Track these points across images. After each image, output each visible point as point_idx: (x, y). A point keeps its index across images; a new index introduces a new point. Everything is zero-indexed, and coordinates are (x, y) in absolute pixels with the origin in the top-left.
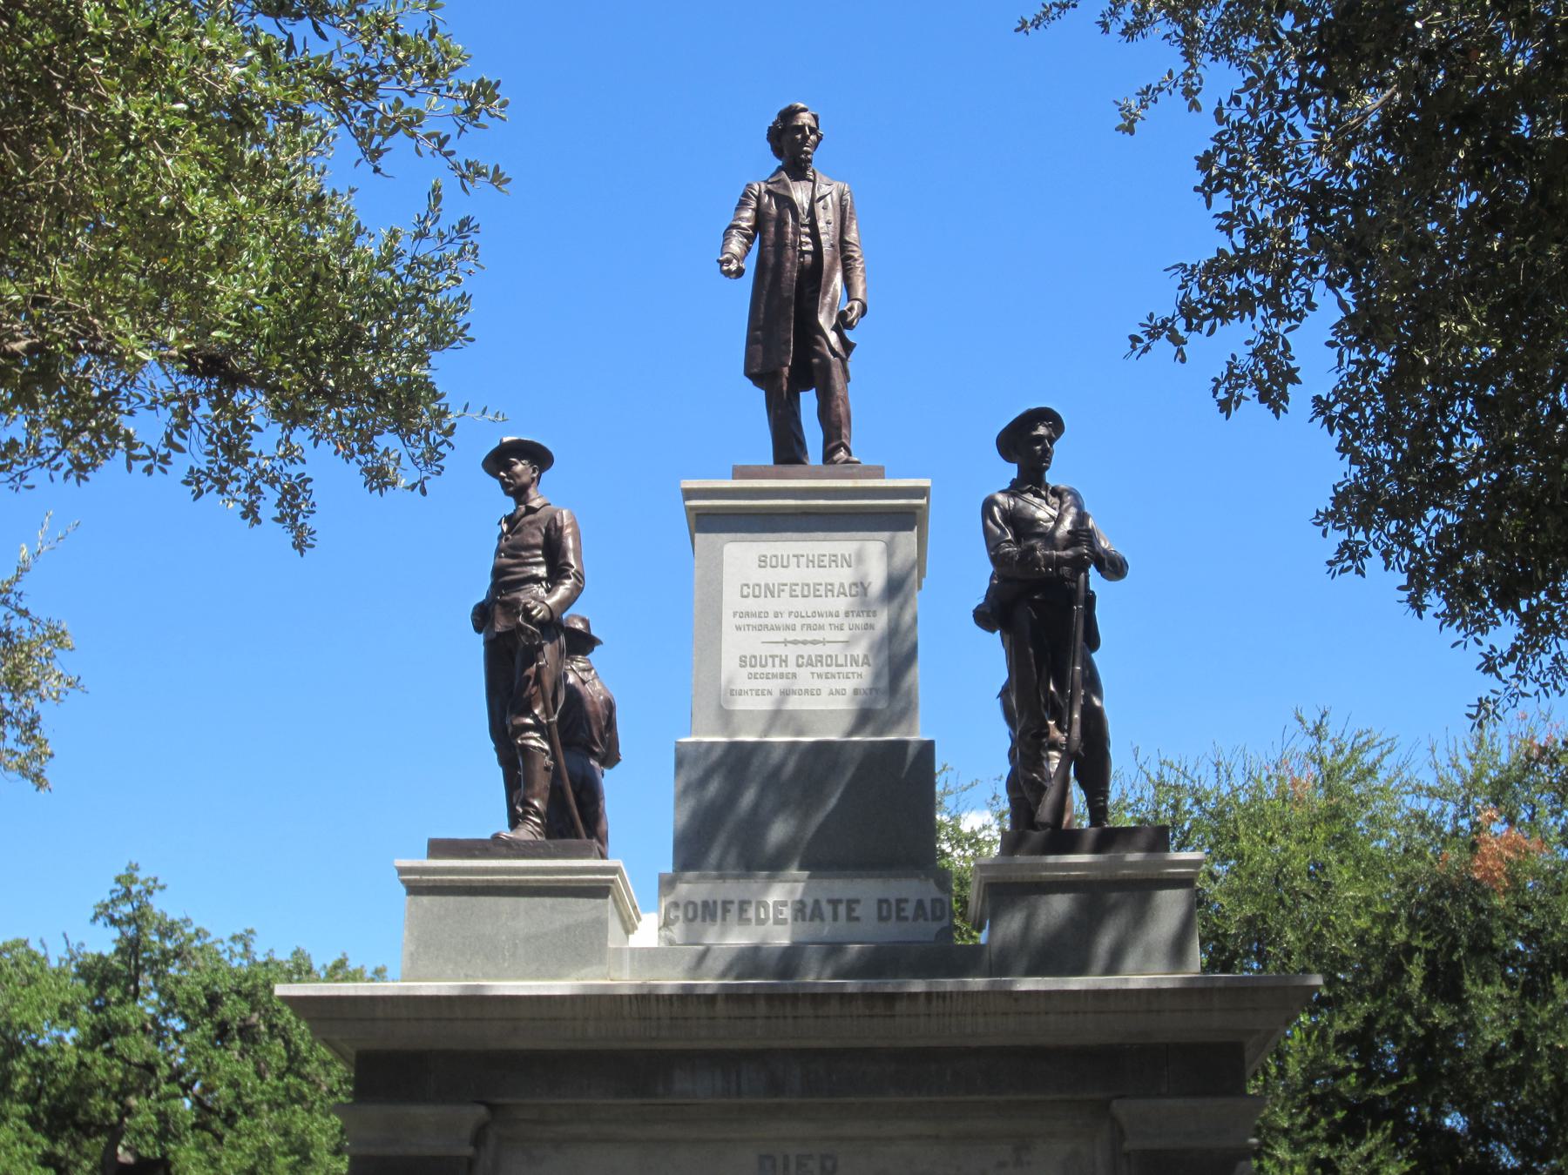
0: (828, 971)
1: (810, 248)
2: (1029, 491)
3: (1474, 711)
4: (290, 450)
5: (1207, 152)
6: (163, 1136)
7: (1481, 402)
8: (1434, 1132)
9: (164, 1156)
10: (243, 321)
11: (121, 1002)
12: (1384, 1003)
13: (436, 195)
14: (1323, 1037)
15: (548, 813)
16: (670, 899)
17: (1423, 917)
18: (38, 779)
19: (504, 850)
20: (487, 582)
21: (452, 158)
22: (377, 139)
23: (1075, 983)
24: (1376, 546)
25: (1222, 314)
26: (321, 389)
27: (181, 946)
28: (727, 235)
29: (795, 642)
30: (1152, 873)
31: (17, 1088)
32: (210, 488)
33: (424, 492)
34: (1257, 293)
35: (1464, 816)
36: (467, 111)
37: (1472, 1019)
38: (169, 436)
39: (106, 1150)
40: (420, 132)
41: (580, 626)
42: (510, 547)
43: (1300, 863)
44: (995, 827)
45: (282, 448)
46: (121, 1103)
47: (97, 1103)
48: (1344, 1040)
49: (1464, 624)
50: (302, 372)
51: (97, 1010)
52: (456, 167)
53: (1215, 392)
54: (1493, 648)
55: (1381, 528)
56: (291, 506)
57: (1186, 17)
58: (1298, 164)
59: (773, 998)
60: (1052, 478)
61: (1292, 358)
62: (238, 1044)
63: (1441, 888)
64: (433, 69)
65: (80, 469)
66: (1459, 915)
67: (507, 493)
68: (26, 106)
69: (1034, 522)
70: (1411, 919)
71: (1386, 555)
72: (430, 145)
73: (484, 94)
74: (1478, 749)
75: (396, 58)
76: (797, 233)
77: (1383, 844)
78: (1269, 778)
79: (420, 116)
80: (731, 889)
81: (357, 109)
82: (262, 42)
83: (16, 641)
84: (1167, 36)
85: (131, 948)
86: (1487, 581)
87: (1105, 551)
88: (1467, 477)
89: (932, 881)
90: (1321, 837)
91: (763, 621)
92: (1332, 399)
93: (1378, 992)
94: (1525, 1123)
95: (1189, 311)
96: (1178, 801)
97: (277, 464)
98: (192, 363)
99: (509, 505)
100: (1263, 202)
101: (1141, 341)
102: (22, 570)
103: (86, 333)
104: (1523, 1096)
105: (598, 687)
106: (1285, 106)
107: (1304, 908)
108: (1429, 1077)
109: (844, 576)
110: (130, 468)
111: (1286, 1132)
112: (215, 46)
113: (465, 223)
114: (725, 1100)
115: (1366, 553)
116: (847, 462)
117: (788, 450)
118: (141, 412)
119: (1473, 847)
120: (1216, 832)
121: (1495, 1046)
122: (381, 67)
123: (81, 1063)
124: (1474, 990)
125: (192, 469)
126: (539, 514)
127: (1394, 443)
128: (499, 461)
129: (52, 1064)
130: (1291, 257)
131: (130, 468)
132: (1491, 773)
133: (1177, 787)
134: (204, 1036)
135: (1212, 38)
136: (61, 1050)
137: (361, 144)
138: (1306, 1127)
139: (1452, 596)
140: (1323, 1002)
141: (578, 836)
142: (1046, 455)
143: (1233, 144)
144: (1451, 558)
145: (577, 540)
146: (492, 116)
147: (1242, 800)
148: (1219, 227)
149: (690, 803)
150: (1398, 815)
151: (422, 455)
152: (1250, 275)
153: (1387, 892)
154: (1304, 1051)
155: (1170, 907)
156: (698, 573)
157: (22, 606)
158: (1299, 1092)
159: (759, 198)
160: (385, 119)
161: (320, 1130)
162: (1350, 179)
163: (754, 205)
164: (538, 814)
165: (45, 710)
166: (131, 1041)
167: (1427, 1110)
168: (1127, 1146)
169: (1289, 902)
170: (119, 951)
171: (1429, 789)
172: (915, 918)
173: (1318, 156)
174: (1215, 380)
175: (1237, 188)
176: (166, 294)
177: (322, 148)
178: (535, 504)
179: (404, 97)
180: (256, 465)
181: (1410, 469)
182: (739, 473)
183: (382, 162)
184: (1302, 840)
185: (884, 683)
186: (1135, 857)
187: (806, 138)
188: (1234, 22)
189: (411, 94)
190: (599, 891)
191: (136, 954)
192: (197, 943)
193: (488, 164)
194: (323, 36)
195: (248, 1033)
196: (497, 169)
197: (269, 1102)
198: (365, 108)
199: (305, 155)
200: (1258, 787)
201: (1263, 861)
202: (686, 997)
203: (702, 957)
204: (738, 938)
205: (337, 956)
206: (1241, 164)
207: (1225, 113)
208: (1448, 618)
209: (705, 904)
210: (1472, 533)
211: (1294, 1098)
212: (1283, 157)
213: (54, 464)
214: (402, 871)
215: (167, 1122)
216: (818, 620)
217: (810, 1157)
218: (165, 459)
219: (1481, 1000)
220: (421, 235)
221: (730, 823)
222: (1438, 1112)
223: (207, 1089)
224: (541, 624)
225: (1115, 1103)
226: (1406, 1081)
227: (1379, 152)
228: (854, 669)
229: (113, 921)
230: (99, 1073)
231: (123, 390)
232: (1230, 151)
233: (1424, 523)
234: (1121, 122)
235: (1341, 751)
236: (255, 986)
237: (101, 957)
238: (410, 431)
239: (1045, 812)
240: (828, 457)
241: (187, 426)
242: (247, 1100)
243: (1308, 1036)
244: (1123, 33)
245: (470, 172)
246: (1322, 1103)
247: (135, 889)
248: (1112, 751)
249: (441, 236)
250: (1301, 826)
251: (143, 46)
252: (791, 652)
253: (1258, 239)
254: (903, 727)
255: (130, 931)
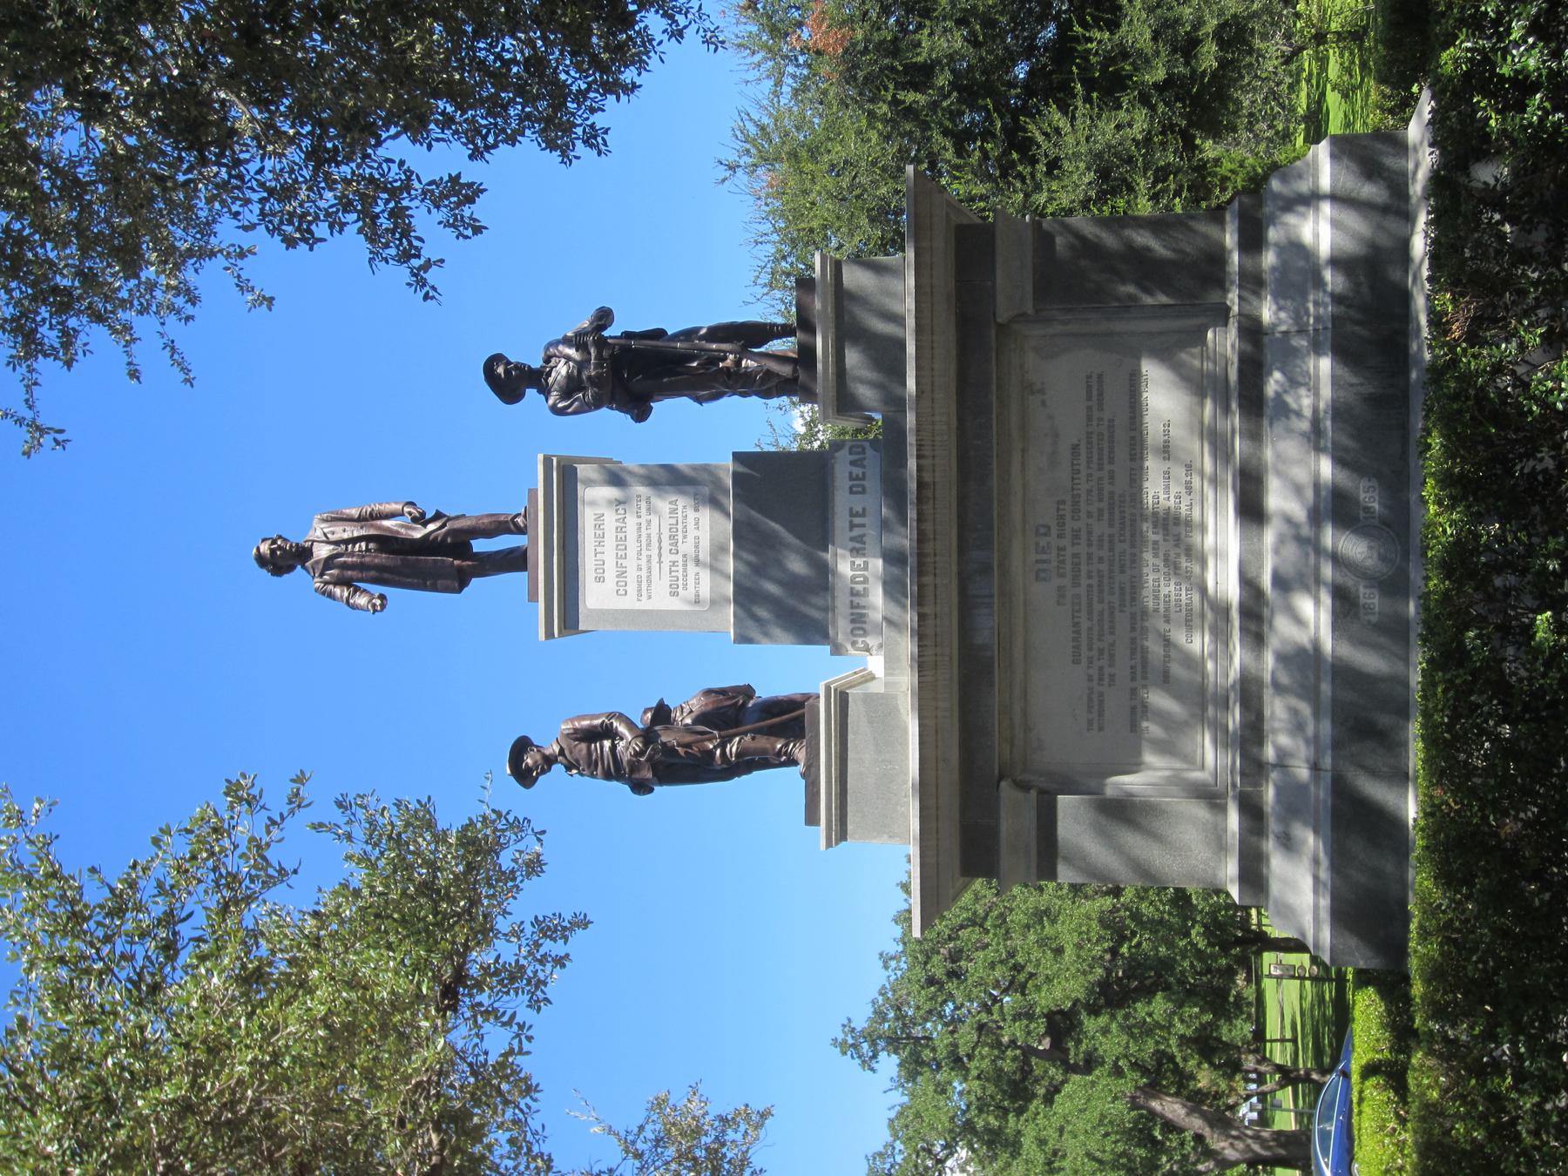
0: (902, 530)
1: (363, 545)
2: (546, 380)
3: (712, 47)
4: (514, 933)
5: (282, 241)
6: (1030, 1016)
7: (480, 33)
8: (1029, 88)
9: (1046, 1016)
10: (414, 970)
11: (934, 1050)
12: (933, 121)
13: (318, 827)
14: (958, 168)
15: (786, 737)
16: (849, 647)
17: (870, 91)
18: (764, 1115)
19: (813, 769)
20: (615, 784)
21: (285, 814)
22: (271, 871)
23: (911, 349)
24: (587, 119)
25: (406, 232)
26: (467, 911)
27: (892, 1007)
28: (354, 607)
29: (660, 555)
30: (830, 291)
31: (997, 1124)
32: (543, 992)
33: (543, 832)
34: (392, 205)
35: (797, 60)
36: (249, 804)
37: (946, 57)
38: (504, 1024)
39: (1041, 1058)
40: (266, 839)
41: (649, 715)
42: (589, 767)
43: (829, 182)
44: (802, 408)
45: (512, 939)
46: (1007, 1048)
47: (1008, 1066)
48: (960, 152)
49: (647, 53)
50: (453, 925)
51: (939, 1067)
52: (292, 812)
53: (467, 237)
54: (665, 31)
55: (573, 114)
56: (556, 931)
57: (181, 255)
58: (292, 171)
59: (920, 571)
60: (536, 363)
61: (441, 179)
62: (962, 963)
63: (850, 79)
64: (215, 830)
65: (529, 1089)
66: (869, 64)
67: (549, 769)
68: (249, 1139)
69: (569, 376)
70: (872, 101)
71: (593, 111)
72: (275, 832)
73: (236, 791)
74: (746, 48)
75: (207, 859)
76: (352, 554)
77: (816, 120)
78: (767, 205)
79: (252, 839)
80: (842, 602)
81: (247, 888)
82: (195, 961)
83: (662, 1134)
84: (196, 271)
85: (894, 1043)
86: (614, 35)
87: (591, 323)
88: (534, 47)
89: (837, 454)
90: (810, 166)
91: (644, 579)
92: (471, 146)
93: (925, 126)
94: (1023, 19)
95: (405, 256)
96: (784, 272)
97: (524, 942)
98: (448, 1007)
99: (558, 769)
100: (321, 198)
101: (427, 293)
102: (610, 1131)
103: (424, 1089)
104: (1004, 20)
105: (695, 701)
106: (240, 177)
107: (863, 179)
108: (989, 90)
109: (610, 518)
110: (528, 1053)
111: (1027, 196)
112: (196, 997)
113: (340, 804)
114: (996, 607)
115: (592, 126)
116: (525, 516)
117: (516, 561)
118: (485, 1045)
119: (819, 53)
120: (807, 244)
121: (966, 39)
122: (215, 869)
123: (978, 1077)
124: (924, 55)
125: (528, 1006)
126: (564, 746)
127: (509, 103)
128: (524, 776)
129: (978, 1099)
130: (364, 178)
131: (528, 1053)
132: (765, 38)
133: (773, 274)
134: (958, 988)
135: (198, 236)
136: (969, 1093)
137: (275, 884)
138: (1023, 180)
139: (625, 63)
140: (933, 165)
141: (803, 715)
142: (518, 367)
143: (276, 221)
144: (596, 63)
145: (583, 717)
146: (253, 785)
147: (783, 225)
148: (340, 232)
149: (777, 632)
150: (795, 109)
151: (516, 834)
152: (378, 210)
153: (853, 120)
154: (967, 182)
155: (855, 277)
156: (609, 628)
157: (636, 1130)
158: (997, 184)
159: (326, 583)
160: (255, 867)
161: (1025, 902)
162: (304, 132)
163: (331, 587)
164: (787, 745)
165: (715, 1110)
166: (961, 1042)
167: (1013, 92)
168: (1030, 311)
169: (858, 191)
170: (896, 1052)
171: (776, 85)
172: (864, 467)
173: (284, 155)
174: (457, 237)
175: (309, 218)
176: (395, 1028)
177: (284, 914)
178: (557, 749)
179: (238, 852)
180: (525, 958)
181: (528, 92)
182: (533, 597)
183: (289, 867)
184: (813, 180)
185: (690, 489)
186: (818, 305)
187: (280, 548)
188: (185, 219)
189: (236, 847)
190: (843, 699)
191: (898, 1039)
192: (890, 995)
193: (290, 788)
194: (191, 914)
195: (955, 957)
196: (293, 781)
197: (1005, 940)
198: (247, 882)
199: (289, 926)
200: (773, 212)
201: (828, 210)
202: (921, 636)
203: (889, 621)
204: (877, 597)
205: (899, 890)
206: (292, 215)
207: (247, 223)
208: (642, 66)
209: (853, 621)
210: (577, 44)
211: (1002, 189)
212: (286, 182)
213: (526, 1110)
214: (829, 845)
215: (1020, 1014)
216: (644, 539)
217: (1037, 544)
218: (521, 1026)
219: (932, 50)
220: (349, 837)
221: (791, 602)
222: (1012, 84)
223: (997, 985)
224: (646, 744)
225: (999, 320)
226: (991, 106)
227: (282, 109)
228: (680, 511)
229: (875, 1056)
230: (985, 1064)
231: (469, 1060)
232: (281, 222)
233: (569, 82)
234: (264, 306)
235: (748, 151)
236: (921, 952)
237: (900, 1065)
238: (498, 843)
239: (785, 370)
240: (521, 531)
241: (495, 1010)
242: (1004, 956)
243: (957, 178)
244: (194, 304)
245: (296, 802)
246: (1006, 169)
247: (850, 1041)
248: (740, 320)
249: (350, 822)
250: (802, 181)
251: (198, 1052)
252: (667, 558)
253: (350, 203)
254: (722, 474)
255: (882, 1043)
